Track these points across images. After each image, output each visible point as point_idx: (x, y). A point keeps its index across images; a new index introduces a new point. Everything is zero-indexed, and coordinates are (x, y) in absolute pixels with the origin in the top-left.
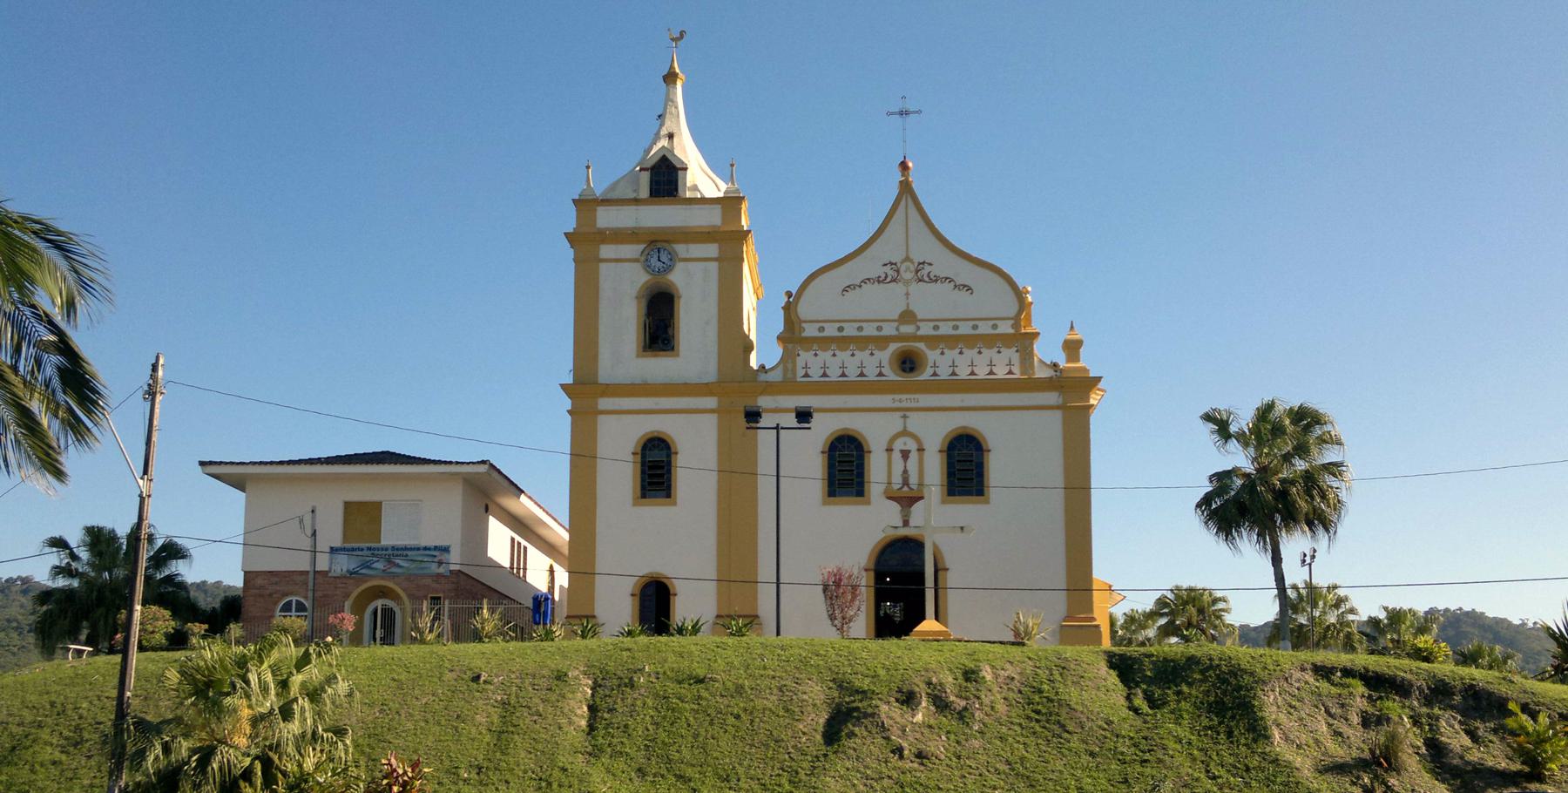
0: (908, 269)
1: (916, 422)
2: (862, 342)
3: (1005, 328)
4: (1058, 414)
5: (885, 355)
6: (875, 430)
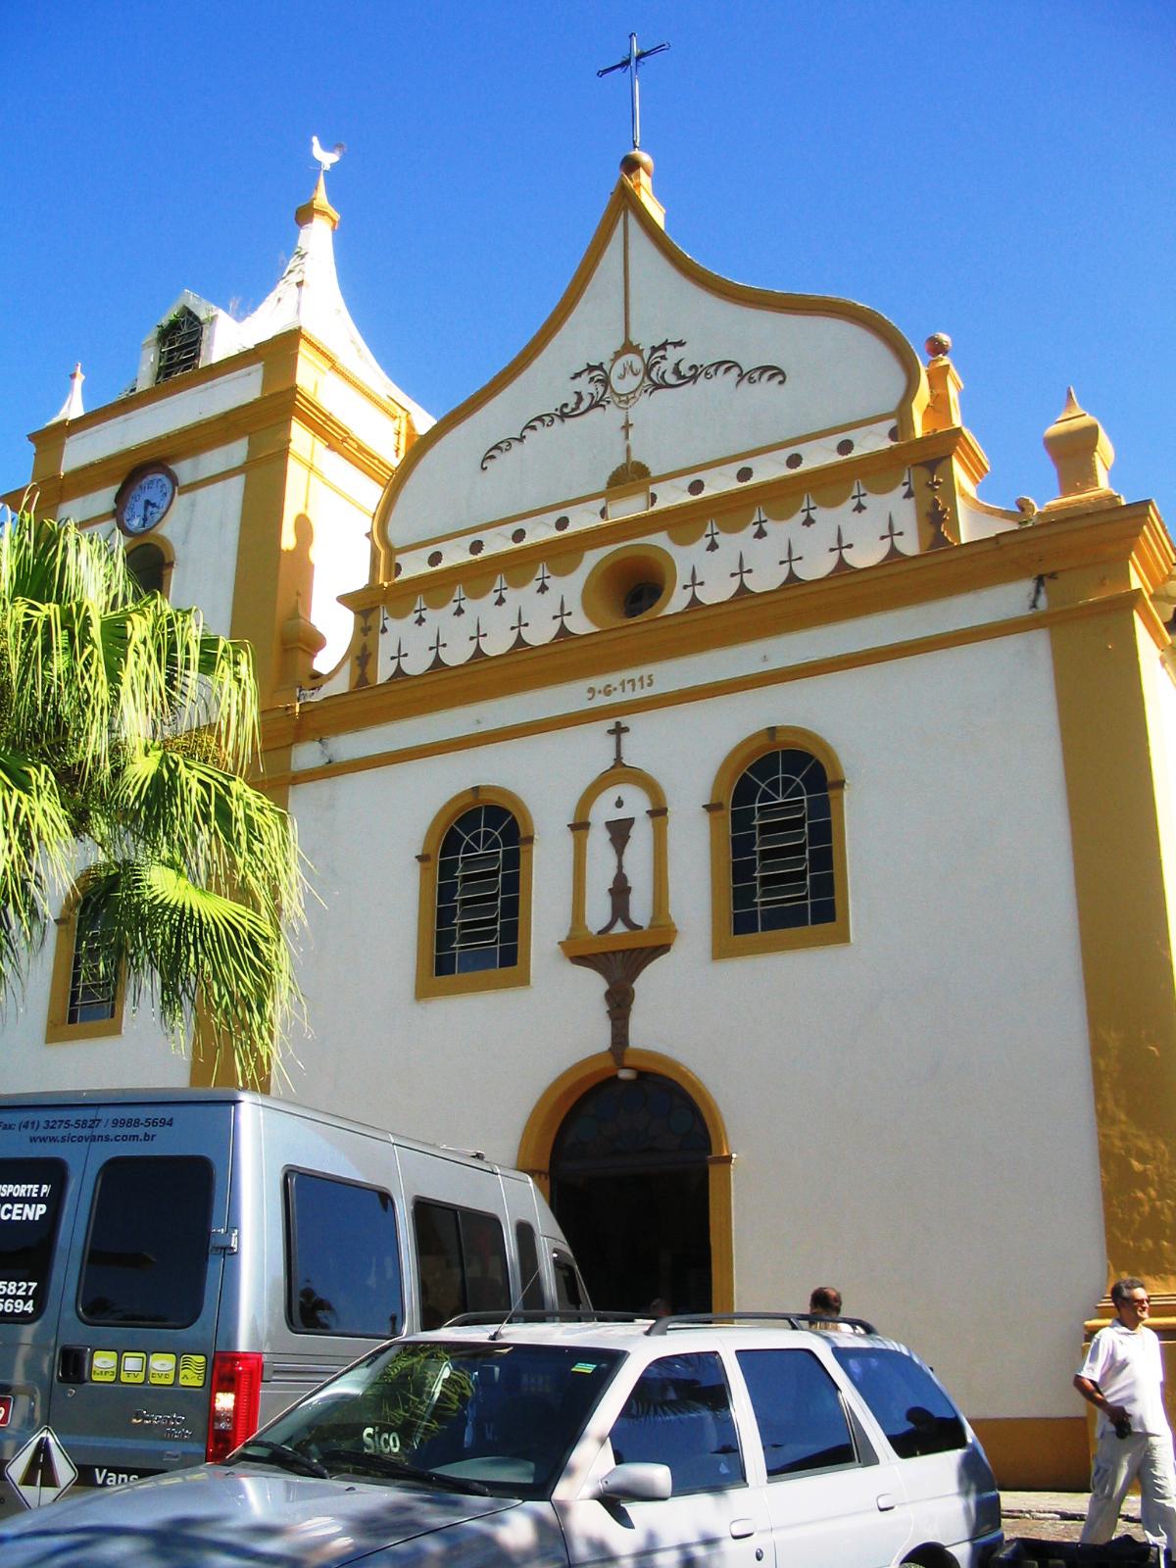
0: (629, 369)
1: (652, 742)
2: (519, 565)
3: (872, 442)
4: (1039, 643)
5: (570, 588)
6: (546, 778)
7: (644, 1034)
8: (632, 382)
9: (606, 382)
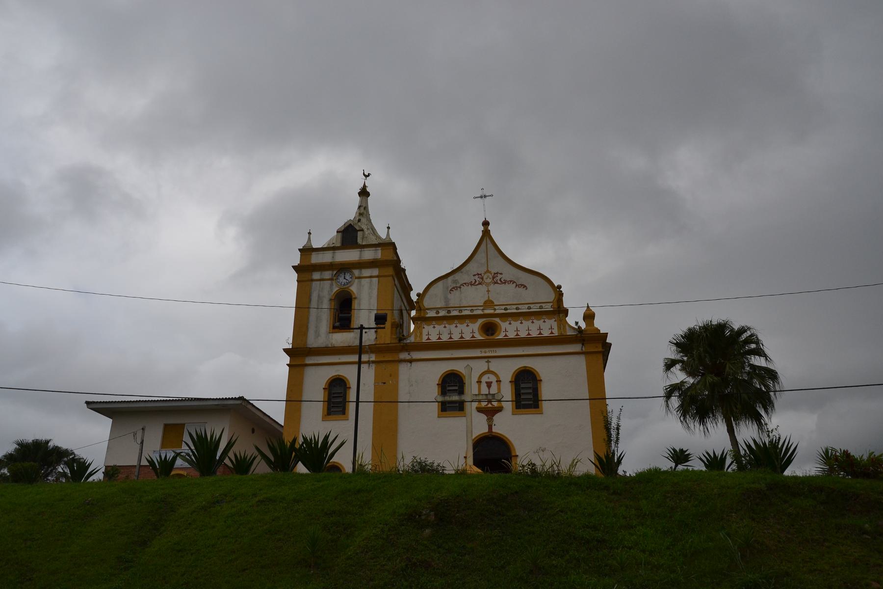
5: (476, 326)
7: (495, 430)
8: (489, 281)
9: (482, 278)
